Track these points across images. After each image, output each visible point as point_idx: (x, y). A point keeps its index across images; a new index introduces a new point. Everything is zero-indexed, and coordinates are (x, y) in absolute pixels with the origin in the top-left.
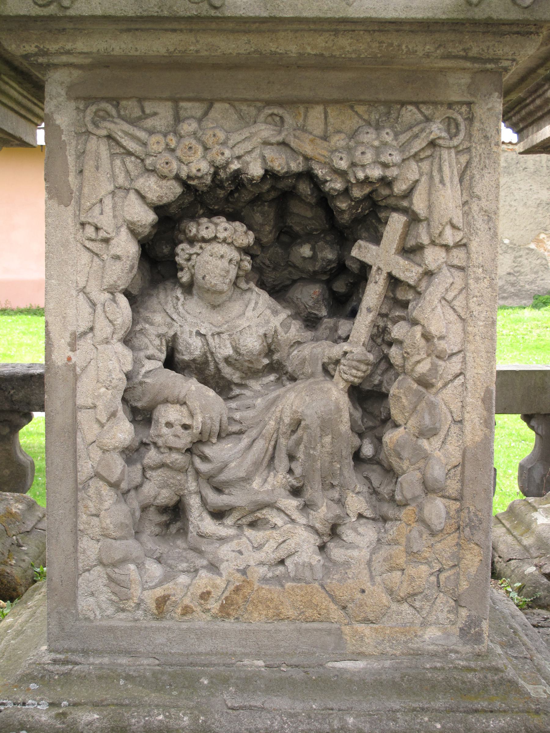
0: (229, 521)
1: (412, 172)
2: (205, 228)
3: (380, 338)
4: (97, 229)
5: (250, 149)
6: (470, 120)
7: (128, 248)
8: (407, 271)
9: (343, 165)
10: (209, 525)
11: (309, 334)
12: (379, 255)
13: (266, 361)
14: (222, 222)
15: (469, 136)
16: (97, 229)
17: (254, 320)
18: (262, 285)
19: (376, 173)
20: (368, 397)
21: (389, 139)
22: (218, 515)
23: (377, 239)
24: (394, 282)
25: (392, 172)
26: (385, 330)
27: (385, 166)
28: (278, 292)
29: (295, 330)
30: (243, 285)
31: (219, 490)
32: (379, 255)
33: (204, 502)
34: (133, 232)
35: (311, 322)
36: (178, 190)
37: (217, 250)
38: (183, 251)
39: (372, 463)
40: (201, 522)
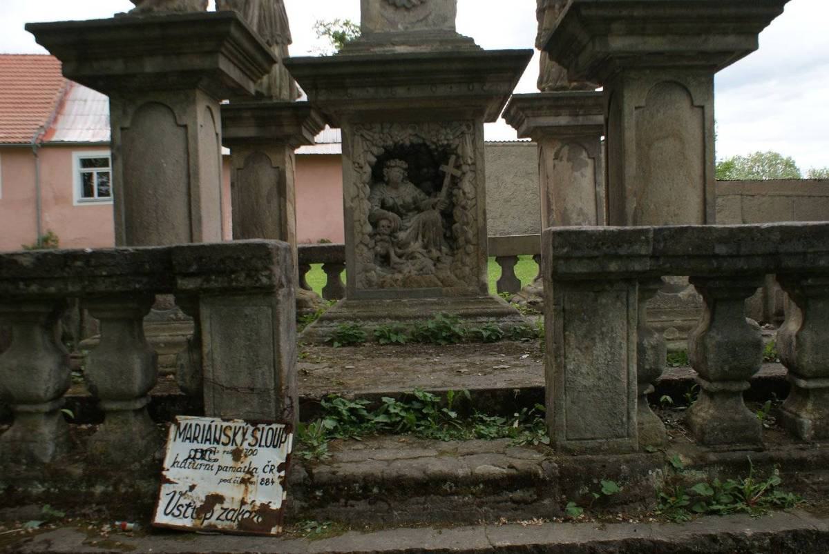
0: (403, 258)
1: (457, 141)
2: (392, 163)
3: (450, 195)
4: (358, 164)
5: (404, 136)
6: (474, 125)
7: (368, 169)
8: (458, 173)
9: (435, 140)
10: (397, 260)
11: (427, 197)
12: (449, 169)
13: (413, 206)
14: (397, 160)
15: (474, 129)
16: (358, 164)
17: (408, 192)
18: (412, 181)
19: (446, 142)
20: (448, 216)
21: (449, 132)
22: (400, 256)
23: (447, 164)
24: (453, 177)
25: (451, 142)
26: (451, 193)
27: (448, 140)
28: (418, 185)
29: (423, 195)
30: (405, 181)
31: (400, 248)
32: (449, 169)
33: (395, 252)
34: (370, 165)
35: (429, 194)
36: (383, 150)
37: (396, 170)
38: (385, 170)
39: (451, 239)
40: (394, 258)
